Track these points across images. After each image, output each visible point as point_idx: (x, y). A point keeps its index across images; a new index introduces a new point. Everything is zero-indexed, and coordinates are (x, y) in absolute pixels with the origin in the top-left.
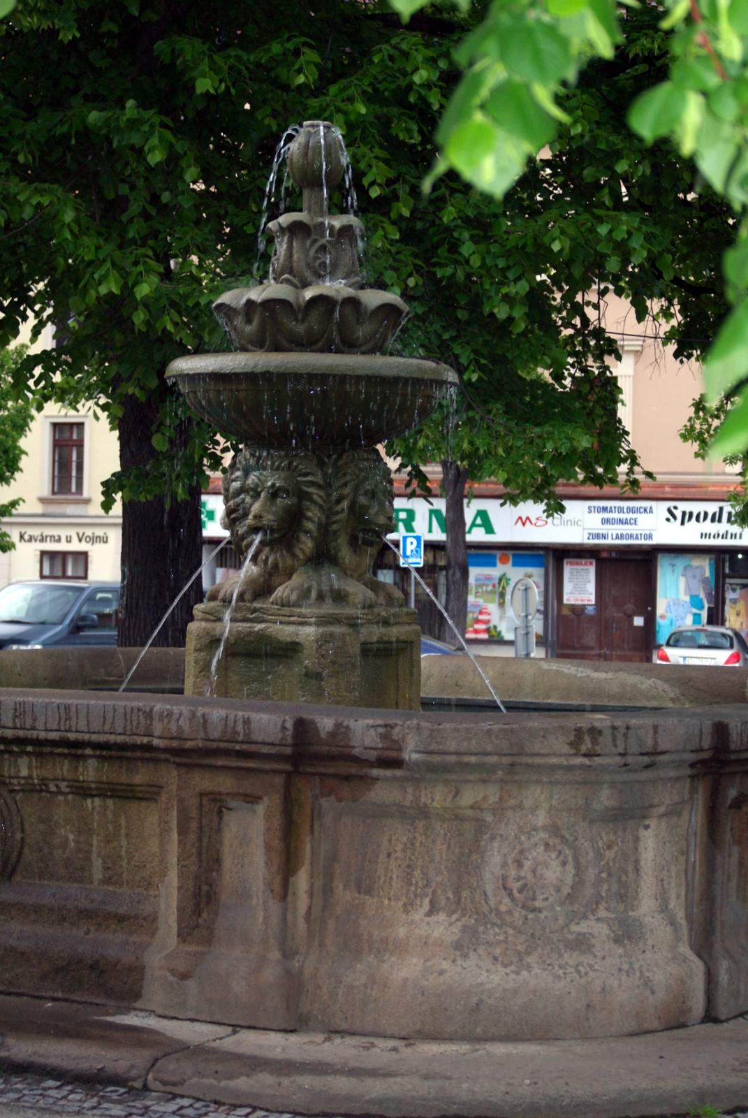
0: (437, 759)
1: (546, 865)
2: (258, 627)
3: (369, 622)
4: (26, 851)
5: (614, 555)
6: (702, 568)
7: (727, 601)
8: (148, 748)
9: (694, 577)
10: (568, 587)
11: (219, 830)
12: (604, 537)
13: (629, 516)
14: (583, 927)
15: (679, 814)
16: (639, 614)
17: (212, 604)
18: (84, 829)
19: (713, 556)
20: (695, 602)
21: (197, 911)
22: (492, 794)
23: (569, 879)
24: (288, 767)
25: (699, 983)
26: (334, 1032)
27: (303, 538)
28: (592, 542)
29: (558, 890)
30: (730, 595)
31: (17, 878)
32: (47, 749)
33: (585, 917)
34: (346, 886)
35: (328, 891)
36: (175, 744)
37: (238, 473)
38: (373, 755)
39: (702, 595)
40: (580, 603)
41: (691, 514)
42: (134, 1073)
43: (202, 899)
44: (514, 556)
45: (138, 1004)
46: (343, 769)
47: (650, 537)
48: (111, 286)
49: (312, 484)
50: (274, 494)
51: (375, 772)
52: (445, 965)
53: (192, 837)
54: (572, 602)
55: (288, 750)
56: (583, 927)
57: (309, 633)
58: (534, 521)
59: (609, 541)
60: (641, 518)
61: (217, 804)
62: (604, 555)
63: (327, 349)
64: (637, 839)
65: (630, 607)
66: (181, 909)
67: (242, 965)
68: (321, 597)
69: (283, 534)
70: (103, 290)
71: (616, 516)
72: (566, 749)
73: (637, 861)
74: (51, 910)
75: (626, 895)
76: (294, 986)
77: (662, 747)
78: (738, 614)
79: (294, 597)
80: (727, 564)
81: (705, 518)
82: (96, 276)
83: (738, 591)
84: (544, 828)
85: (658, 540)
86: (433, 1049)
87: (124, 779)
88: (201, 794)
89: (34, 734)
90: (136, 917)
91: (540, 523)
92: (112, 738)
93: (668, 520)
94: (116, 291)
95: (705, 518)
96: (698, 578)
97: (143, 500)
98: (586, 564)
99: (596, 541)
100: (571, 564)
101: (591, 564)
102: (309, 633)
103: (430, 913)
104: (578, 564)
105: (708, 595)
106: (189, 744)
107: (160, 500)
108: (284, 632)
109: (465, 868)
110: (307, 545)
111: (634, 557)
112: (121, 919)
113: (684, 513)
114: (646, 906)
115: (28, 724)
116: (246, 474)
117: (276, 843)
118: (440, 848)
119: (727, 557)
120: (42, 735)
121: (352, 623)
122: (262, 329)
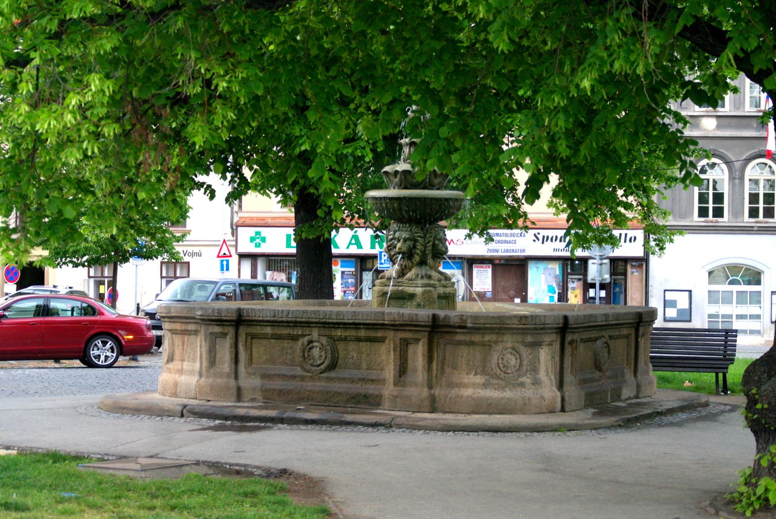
0: (477, 326)
1: (511, 359)
2: (400, 288)
3: (440, 286)
4: (339, 360)
5: (502, 262)
6: (555, 269)
7: (569, 289)
8: (383, 324)
9: (550, 274)
10: (475, 280)
11: (407, 351)
12: (497, 251)
13: (512, 238)
14: (521, 380)
15: (552, 345)
16: (517, 297)
17: (383, 280)
18: (360, 353)
19: (561, 262)
20: (551, 289)
21: (400, 376)
22: (494, 337)
23: (518, 364)
24: (429, 329)
25: (559, 399)
26: (445, 412)
27: (416, 256)
28: (490, 254)
29: (515, 367)
30: (571, 285)
31: (337, 369)
32: (347, 326)
33: (523, 376)
34: (448, 367)
35: (443, 369)
36: (392, 323)
37: (392, 233)
38: (457, 324)
39: (555, 285)
40: (482, 290)
41: (548, 237)
42: (387, 422)
43: (402, 370)
44: (342, 262)
45: (380, 407)
46: (446, 330)
47: (524, 251)
48: (306, 147)
49: (420, 237)
50: (405, 240)
51: (458, 330)
52: (480, 391)
53: (398, 353)
54: (478, 290)
55: (430, 324)
56: (521, 380)
57: (419, 290)
58: (455, 242)
59: (500, 254)
60: (519, 240)
61: (405, 344)
62: (497, 262)
63: (425, 188)
64: (539, 352)
65: (512, 293)
66: (394, 376)
67: (417, 391)
68: (422, 277)
69: (409, 255)
70: (303, 148)
71: (504, 238)
72: (517, 322)
73: (539, 359)
74: (349, 379)
75: (535, 370)
76: (433, 399)
77: (547, 322)
78: (576, 296)
79: (413, 277)
80: (569, 267)
81: (556, 240)
82: (300, 142)
83: (576, 283)
84: (511, 348)
85: (528, 253)
86: (477, 416)
87: (374, 335)
88: (401, 339)
89: (343, 321)
90: (378, 380)
91: (459, 243)
92: (371, 322)
93: (534, 241)
94: (309, 149)
95: (556, 240)
96: (552, 275)
97: (311, 238)
98: (486, 267)
99: (492, 254)
100: (477, 267)
101: (489, 267)
102: (419, 290)
103: (475, 375)
104: (481, 267)
105: (558, 285)
106: (398, 323)
107: (319, 238)
108: (411, 290)
109: (485, 360)
110: (417, 258)
111: (514, 263)
112: (373, 381)
113: (544, 237)
114: (542, 375)
115: (341, 318)
116: (395, 232)
117: (426, 353)
118: (478, 354)
119: (569, 262)
120: (346, 321)
121: (433, 286)
122: (401, 180)
